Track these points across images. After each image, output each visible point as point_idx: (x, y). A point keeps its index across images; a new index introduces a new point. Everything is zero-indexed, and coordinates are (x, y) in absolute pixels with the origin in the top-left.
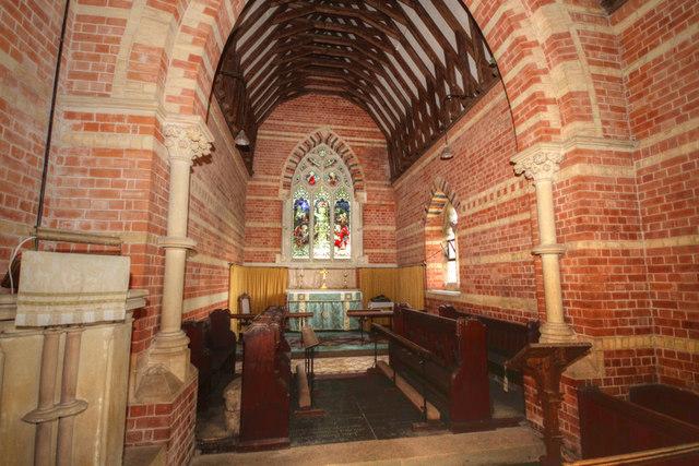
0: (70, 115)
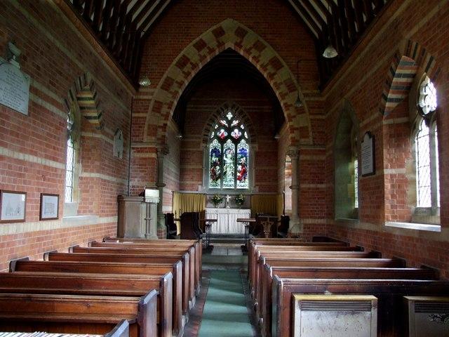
0: (133, 148)
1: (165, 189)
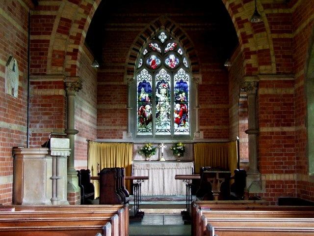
0: (33, 83)
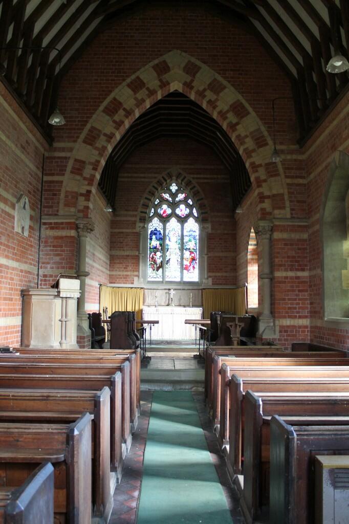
0: (45, 224)
1: (88, 281)
